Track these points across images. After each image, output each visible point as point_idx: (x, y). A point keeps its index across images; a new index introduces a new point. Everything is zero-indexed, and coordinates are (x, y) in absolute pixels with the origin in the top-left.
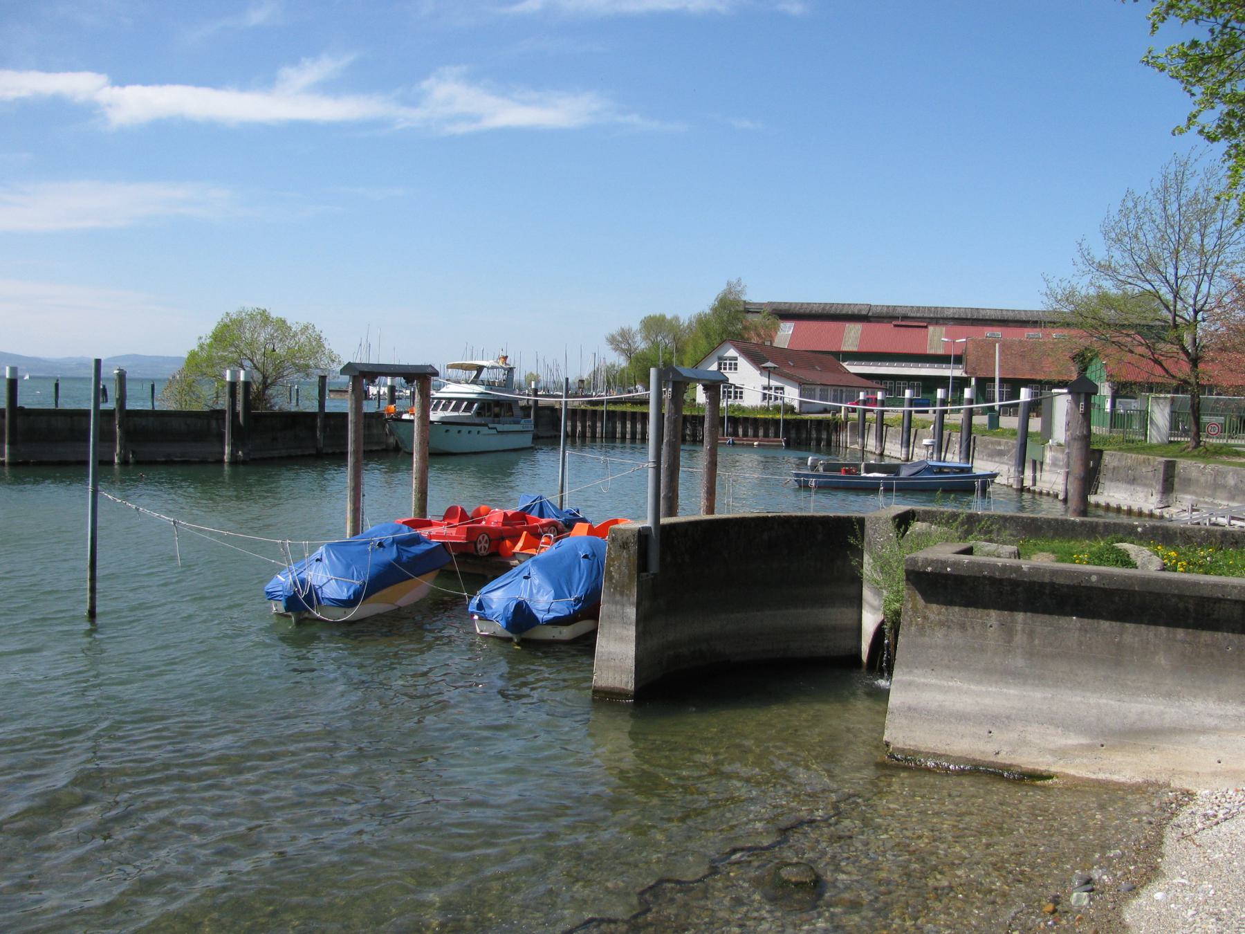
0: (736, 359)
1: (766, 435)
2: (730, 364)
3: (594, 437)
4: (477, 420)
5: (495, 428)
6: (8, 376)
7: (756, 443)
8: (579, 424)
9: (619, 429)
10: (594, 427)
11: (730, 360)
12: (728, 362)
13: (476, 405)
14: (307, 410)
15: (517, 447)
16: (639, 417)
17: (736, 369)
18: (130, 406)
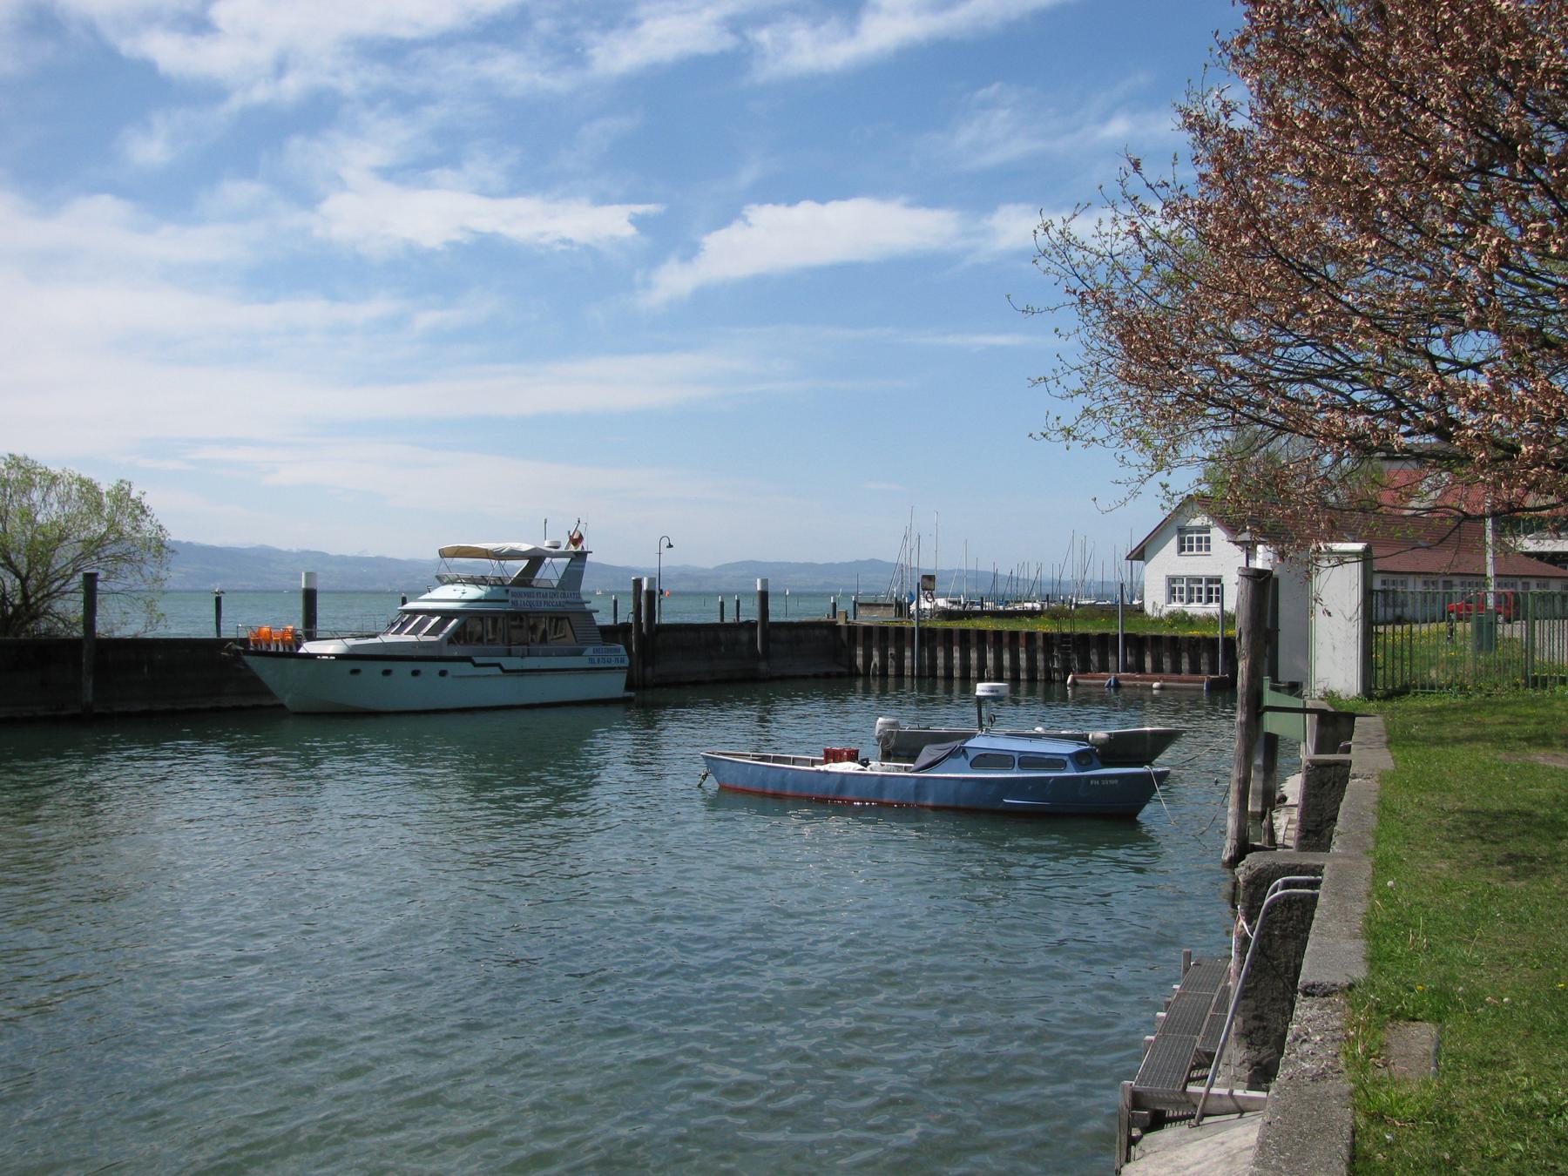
0: (1207, 529)
1: (1176, 669)
2: (1199, 540)
3: (900, 675)
4: (456, 651)
5: (498, 665)
6: (759, 588)
7: (1156, 685)
8: (875, 653)
9: (940, 661)
10: (900, 658)
11: (1198, 532)
12: (1195, 536)
13: (455, 621)
14: (117, 634)
15: (536, 701)
16: (973, 639)
17: (1208, 548)
18: (772, 619)
